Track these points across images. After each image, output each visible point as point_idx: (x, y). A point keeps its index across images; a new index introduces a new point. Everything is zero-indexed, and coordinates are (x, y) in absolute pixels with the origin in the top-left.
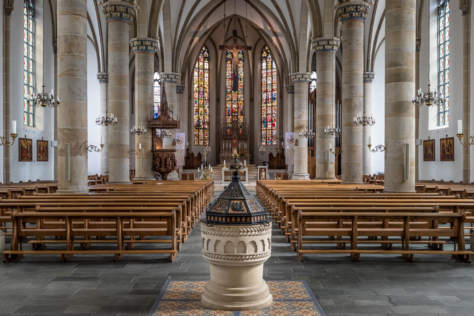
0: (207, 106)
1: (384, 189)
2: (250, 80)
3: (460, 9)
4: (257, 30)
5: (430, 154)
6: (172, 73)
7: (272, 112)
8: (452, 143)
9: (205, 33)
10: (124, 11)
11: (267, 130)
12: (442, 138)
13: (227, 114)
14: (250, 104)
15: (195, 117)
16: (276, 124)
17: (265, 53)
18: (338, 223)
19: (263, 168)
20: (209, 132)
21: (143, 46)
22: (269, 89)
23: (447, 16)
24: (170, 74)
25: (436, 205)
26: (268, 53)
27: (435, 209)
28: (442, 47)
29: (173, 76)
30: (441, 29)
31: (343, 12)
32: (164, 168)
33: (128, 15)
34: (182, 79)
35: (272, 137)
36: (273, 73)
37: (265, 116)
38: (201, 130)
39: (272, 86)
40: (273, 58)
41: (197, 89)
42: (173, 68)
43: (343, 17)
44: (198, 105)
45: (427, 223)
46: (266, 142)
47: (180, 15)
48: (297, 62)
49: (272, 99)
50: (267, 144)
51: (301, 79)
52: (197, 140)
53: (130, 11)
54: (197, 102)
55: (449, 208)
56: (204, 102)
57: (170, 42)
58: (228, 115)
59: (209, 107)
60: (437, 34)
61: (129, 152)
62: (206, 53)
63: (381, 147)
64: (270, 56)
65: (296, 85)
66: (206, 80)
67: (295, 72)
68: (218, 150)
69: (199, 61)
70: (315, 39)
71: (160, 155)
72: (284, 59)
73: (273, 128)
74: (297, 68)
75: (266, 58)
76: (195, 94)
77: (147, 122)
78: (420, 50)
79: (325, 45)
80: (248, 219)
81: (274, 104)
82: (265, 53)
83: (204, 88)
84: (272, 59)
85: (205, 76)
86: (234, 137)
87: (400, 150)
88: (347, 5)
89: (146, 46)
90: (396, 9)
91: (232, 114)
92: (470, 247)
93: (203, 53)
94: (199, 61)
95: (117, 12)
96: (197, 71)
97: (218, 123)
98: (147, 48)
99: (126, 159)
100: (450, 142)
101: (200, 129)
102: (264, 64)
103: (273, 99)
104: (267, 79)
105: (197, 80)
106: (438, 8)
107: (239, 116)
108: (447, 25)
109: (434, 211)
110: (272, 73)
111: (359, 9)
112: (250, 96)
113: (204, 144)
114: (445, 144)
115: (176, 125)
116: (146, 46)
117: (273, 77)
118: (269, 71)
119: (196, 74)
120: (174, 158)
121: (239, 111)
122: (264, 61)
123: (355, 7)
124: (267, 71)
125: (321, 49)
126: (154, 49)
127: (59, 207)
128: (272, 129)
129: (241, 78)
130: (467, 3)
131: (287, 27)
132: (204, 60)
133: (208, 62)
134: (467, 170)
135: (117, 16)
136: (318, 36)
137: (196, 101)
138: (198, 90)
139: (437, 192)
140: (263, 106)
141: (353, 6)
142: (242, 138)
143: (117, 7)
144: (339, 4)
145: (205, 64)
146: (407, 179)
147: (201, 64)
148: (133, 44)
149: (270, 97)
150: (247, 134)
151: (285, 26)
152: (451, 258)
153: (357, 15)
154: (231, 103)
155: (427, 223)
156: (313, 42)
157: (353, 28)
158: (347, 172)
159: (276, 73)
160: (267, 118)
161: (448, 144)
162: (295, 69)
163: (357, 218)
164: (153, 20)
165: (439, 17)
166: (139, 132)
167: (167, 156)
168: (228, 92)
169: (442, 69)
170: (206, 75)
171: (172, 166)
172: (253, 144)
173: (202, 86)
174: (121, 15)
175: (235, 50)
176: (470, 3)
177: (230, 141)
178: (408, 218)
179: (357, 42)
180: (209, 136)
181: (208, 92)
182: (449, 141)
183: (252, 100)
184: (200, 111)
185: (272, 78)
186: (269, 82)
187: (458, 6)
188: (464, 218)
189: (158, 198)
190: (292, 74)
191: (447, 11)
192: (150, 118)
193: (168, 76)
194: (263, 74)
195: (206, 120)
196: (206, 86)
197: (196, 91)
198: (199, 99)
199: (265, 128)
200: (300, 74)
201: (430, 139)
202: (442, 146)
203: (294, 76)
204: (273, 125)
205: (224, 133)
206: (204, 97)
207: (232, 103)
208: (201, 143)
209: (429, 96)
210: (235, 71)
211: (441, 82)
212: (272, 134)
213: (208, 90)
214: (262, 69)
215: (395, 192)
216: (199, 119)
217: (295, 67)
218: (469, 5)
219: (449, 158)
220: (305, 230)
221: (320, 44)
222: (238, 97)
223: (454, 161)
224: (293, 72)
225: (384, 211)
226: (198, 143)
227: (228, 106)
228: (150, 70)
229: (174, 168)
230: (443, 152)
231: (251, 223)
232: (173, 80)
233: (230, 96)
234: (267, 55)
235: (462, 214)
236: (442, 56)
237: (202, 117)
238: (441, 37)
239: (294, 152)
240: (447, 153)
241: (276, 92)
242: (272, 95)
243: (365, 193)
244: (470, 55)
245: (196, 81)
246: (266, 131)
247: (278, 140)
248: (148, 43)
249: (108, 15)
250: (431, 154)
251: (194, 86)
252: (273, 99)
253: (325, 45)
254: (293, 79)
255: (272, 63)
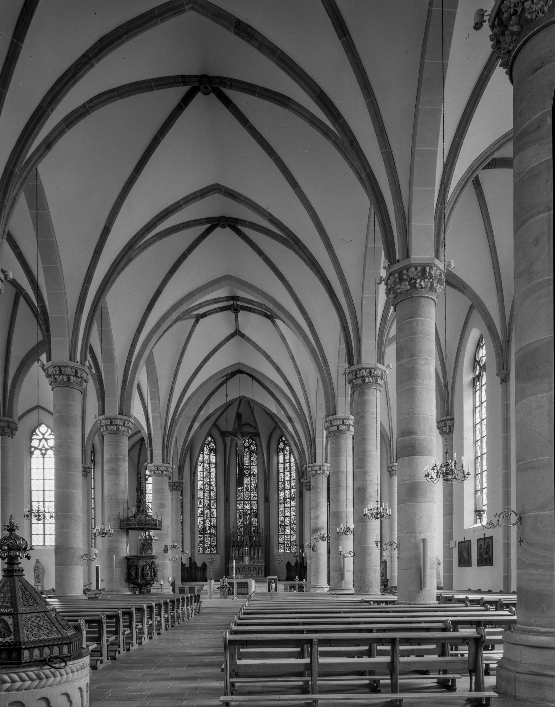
0: (213, 507)
1: (396, 601)
2: (265, 476)
3: (498, 375)
4: (270, 415)
5: (465, 558)
6: (162, 464)
7: (291, 514)
8: (490, 544)
9: (207, 419)
10: (72, 373)
11: (284, 535)
12: (479, 537)
13: (238, 517)
14: (265, 505)
15: (199, 520)
16: (295, 528)
17: (281, 444)
18: (302, 651)
19: (272, 579)
20: (217, 538)
21: (113, 425)
22: (287, 486)
23: (484, 388)
24: (160, 466)
25: (446, 621)
26: (285, 445)
27: (445, 626)
28: (478, 426)
29: (164, 469)
30: (478, 404)
31: (354, 377)
32: (141, 578)
33: (79, 380)
34: (179, 473)
35: (291, 543)
36: (292, 468)
37: (282, 518)
38: (207, 536)
39: (290, 483)
40: (291, 452)
41: (202, 487)
42: (163, 459)
43: (354, 384)
44: (203, 506)
45: (434, 646)
46: (284, 550)
47: (171, 394)
48: (313, 451)
49: (290, 498)
50: (285, 551)
51: (318, 472)
52: (202, 548)
53: (81, 375)
54: (202, 502)
55: (470, 623)
56: (210, 502)
57: (160, 427)
58: (239, 518)
59: (216, 508)
60: (472, 411)
61: (82, 557)
62: (212, 444)
63: (392, 544)
64: (287, 448)
65: (312, 480)
66: (213, 476)
67: (312, 463)
68: (227, 560)
69: (203, 454)
70: (327, 418)
71: (135, 563)
72: (302, 449)
73: (292, 533)
74: (313, 458)
75: (283, 450)
76: (199, 493)
77: (119, 522)
78: (454, 432)
79: (339, 425)
80: (14, 655)
81: (292, 505)
82: (281, 444)
83: (210, 485)
84: (290, 452)
85: (211, 471)
86: (245, 544)
87: (416, 547)
88: (358, 367)
89: (118, 426)
90: (409, 359)
91: (244, 516)
92: (497, 683)
93: (209, 444)
94: (203, 454)
95: (63, 375)
96: (202, 465)
97: (227, 527)
98: (118, 429)
99: (77, 566)
100: (488, 543)
101: (206, 534)
102: (281, 458)
103: (291, 498)
104: (284, 474)
105: (202, 476)
106: (474, 379)
107: (252, 519)
108: (484, 399)
109: (444, 630)
110: (290, 467)
111: (374, 373)
112: (265, 495)
113: (210, 552)
114: (483, 545)
115: (156, 525)
116: (118, 426)
117: (292, 472)
118: (287, 465)
119: (200, 468)
120: (153, 567)
121: (253, 513)
122: (281, 453)
123: (368, 371)
124: (284, 465)
125: (334, 430)
126: (128, 430)
127: (362, 624)
128: (291, 534)
129: (254, 474)
130: (505, 368)
131: (301, 408)
132: (210, 452)
133: (214, 454)
134: (508, 576)
135: (62, 380)
136: (331, 415)
137: (201, 501)
138: (202, 488)
139: (483, 605)
140: (280, 507)
141: (365, 369)
142: (255, 545)
143: (63, 369)
144: (349, 367)
145: (212, 457)
146: (424, 587)
147: (206, 457)
148: (101, 423)
149: (288, 496)
150: (261, 540)
151: (299, 408)
152: (465, 702)
153: (371, 381)
154: (242, 503)
155: (434, 646)
156: (326, 422)
157: (366, 398)
158: (361, 580)
159: (294, 467)
160: (285, 521)
161: (486, 544)
162: (312, 459)
163: (317, 643)
164: (125, 394)
165: (474, 390)
166: (103, 533)
167: (144, 564)
168: (239, 490)
169: (479, 454)
170: (213, 470)
171: (152, 577)
172: (269, 552)
173: (207, 484)
174: (69, 379)
175: (240, 437)
176: (509, 369)
177: (237, 548)
178: (397, 642)
179: (371, 415)
180: (217, 543)
181: (215, 490)
182: (487, 541)
183: (267, 500)
184: (205, 514)
185: (290, 474)
186: (287, 478)
187: (496, 372)
188: (483, 639)
189: (298, 618)
190: (308, 465)
191: (484, 381)
192: (123, 517)
193: (158, 468)
194: (280, 469)
195: (212, 524)
196: (212, 483)
197: (201, 489)
198: (204, 499)
199: (283, 533)
200: (318, 466)
201: (466, 540)
202: (479, 548)
203: (311, 468)
204: (291, 529)
205: (233, 538)
206: (210, 496)
207: (244, 504)
208: (207, 551)
209: (447, 468)
210: (240, 463)
211: (477, 470)
212: (291, 540)
213: (215, 488)
214: (278, 464)
215: (409, 604)
216: (204, 523)
217: (312, 457)
218: (508, 371)
219: (487, 562)
220: (236, 664)
221: (333, 424)
222: (251, 496)
223: (493, 565)
224: (309, 463)
225: (370, 631)
226: (204, 551)
227: (239, 507)
228: (122, 455)
229: (153, 579)
230: (480, 554)
231: (21, 663)
232: (164, 473)
233: (241, 495)
234: (285, 447)
235: (480, 634)
236: (478, 438)
237: (207, 520)
238: (478, 415)
239: (312, 559)
240: (485, 556)
241: (295, 490)
242: (290, 493)
243: (370, 605)
244: (510, 432)
245: (201, 478)
246: (284, 536)
247: (298, 547)
248: (119, 422)
249: (51, 378)
250: (467, 558)
251: (198, 483)
252: (291, 498)
253: (339, 425)
254: (309, 472)
255: (290, 456)
